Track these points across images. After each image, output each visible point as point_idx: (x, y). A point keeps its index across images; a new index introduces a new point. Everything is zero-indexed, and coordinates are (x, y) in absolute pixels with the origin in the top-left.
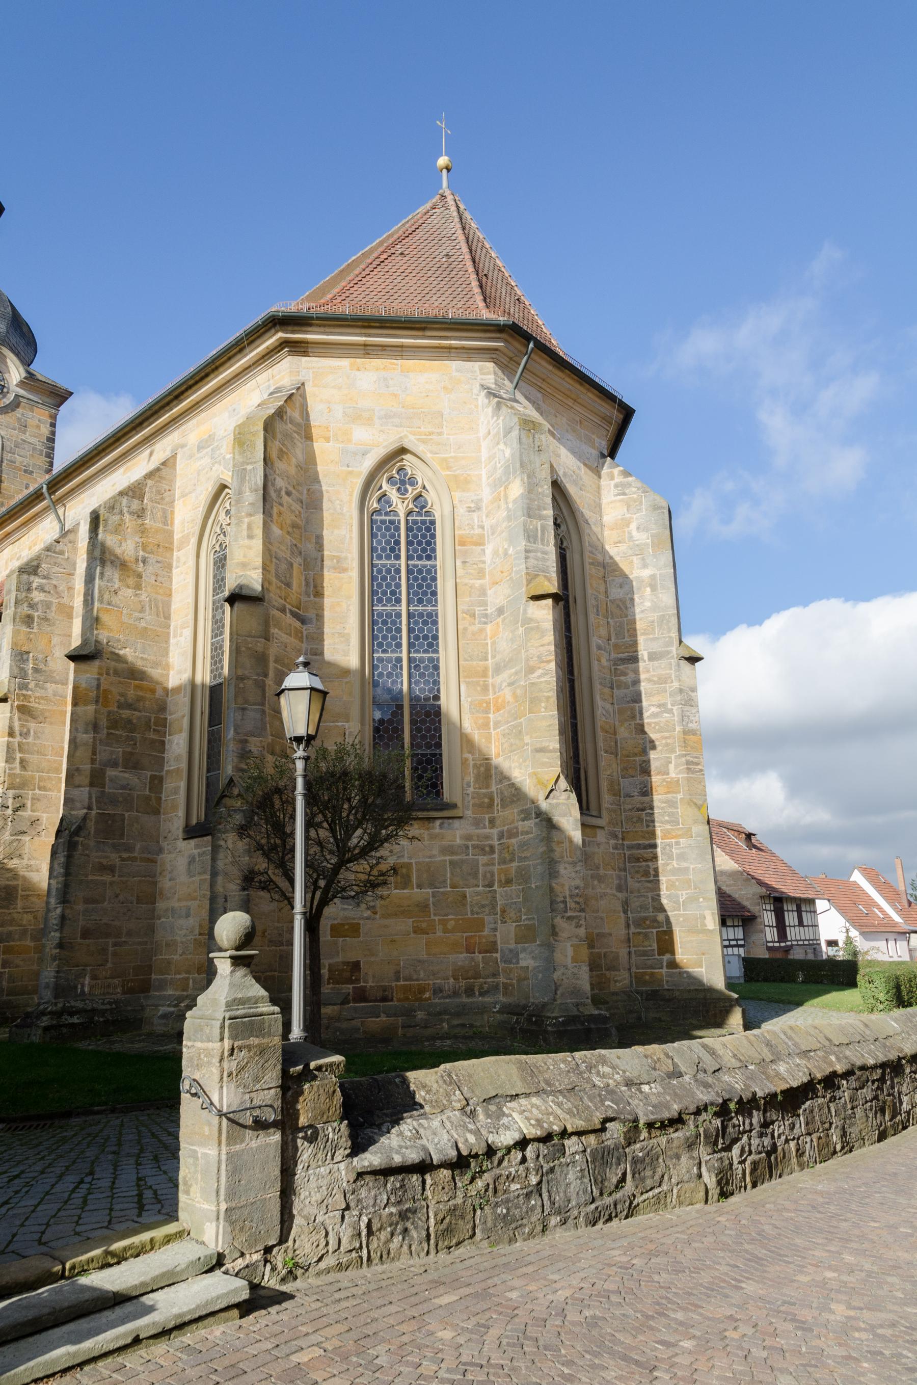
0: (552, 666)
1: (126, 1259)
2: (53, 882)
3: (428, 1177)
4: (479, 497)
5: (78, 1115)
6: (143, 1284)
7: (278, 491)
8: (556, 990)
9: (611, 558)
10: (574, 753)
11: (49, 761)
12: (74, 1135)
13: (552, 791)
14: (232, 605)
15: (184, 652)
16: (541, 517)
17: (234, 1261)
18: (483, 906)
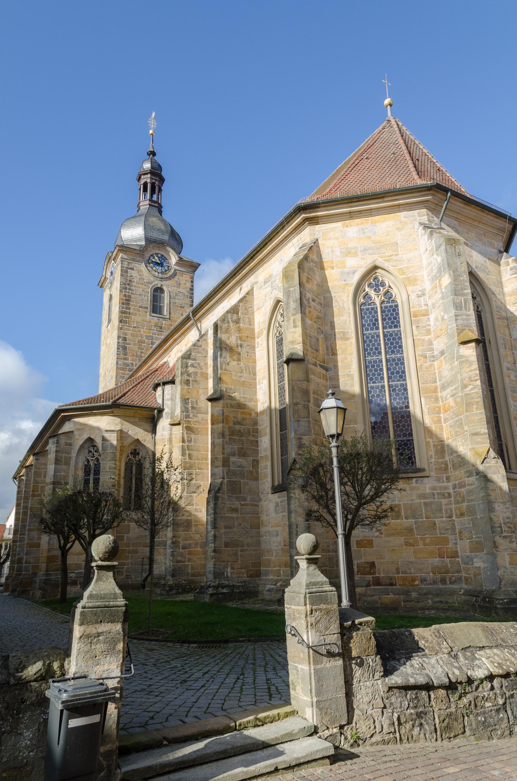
0: (479, 382)
1: (266, 723)
2: (209, 517)
3: (431, 693)
4: (423, 288)
5: (232, 642)
6: (276, 738)
7: (308, 300)
8: (500, 582)
9: (512, 313)
10: (497, 435)
11: (202, 454)
12: (231, 653)
13: (485, 458)
14: (288, 365)
15: (265, 392)
16: (463, 295)
17: (323, 731)
18: (447, 529)
